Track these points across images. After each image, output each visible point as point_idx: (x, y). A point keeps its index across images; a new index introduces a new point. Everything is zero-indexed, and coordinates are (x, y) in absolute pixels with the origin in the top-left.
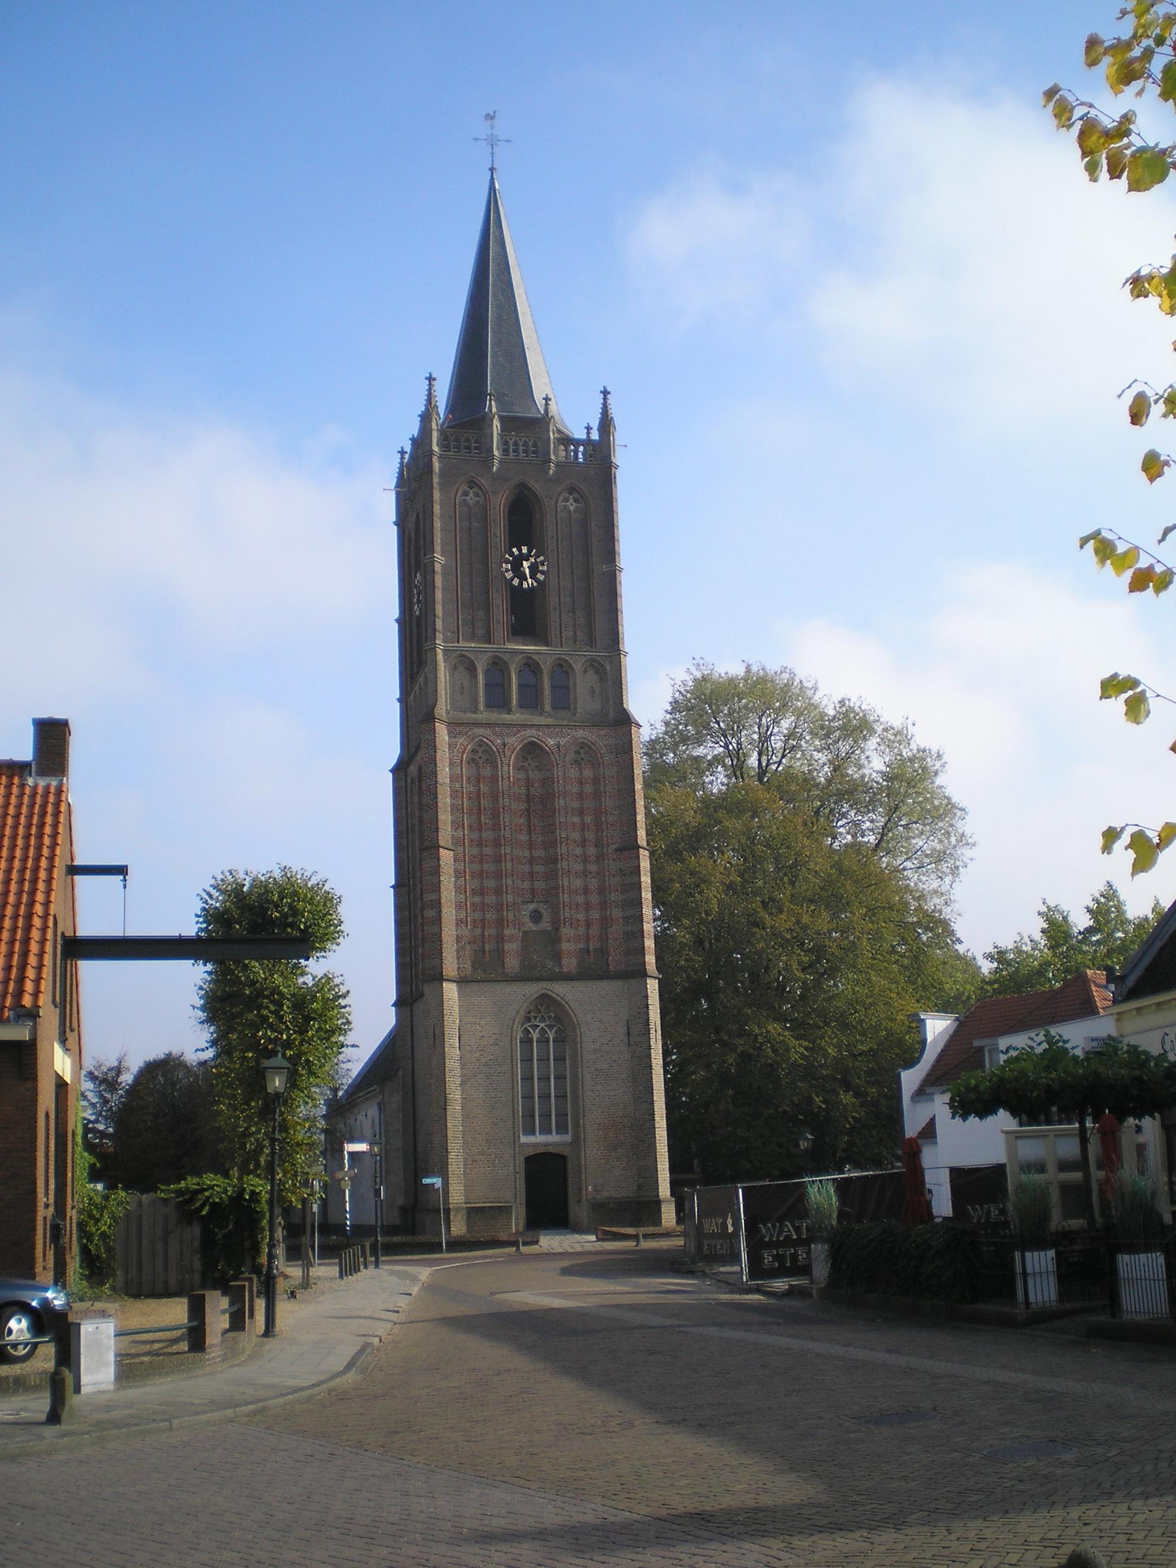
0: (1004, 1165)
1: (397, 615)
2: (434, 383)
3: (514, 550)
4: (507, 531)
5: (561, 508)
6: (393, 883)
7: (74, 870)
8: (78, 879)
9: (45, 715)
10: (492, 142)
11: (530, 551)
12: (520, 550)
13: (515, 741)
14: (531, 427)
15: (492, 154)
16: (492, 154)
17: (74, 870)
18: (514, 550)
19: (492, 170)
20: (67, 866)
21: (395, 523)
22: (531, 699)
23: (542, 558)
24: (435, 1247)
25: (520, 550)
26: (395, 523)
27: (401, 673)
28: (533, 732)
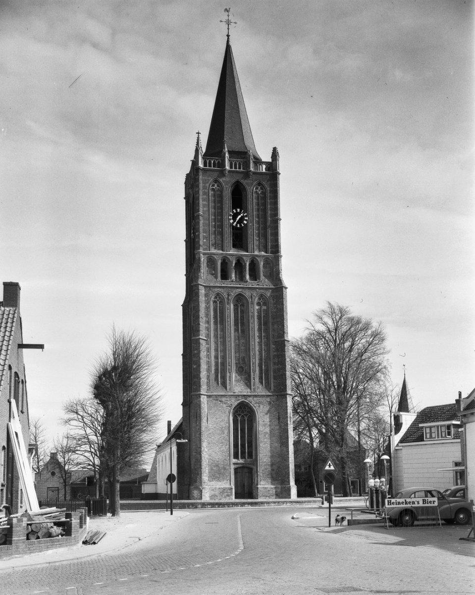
0: (290, 498)
1: (182, 353)
2: (200, 135)
3: (234, 210)
4: (233, 204)
5: (252, 192)
6: (184, 197)
7: (22, 346)
8: (25, 350)
9: (5, 281)
10: (228, 23)
11: (241, 211)
12: (236, 210)
13: (233, 294)
14: (243, 155)
15: (228, 29)
16: (228, 29)
17: (22, 346)
18: (234, 210)
19: (228, 36)
20: (19, 345)
21: (185, 198)
22: (239, 264)
23: (246, 214)
24: (194, 506)
25: (236, 210)
26: (185, 198)
27: (186, 228)
28: (240, 290)
